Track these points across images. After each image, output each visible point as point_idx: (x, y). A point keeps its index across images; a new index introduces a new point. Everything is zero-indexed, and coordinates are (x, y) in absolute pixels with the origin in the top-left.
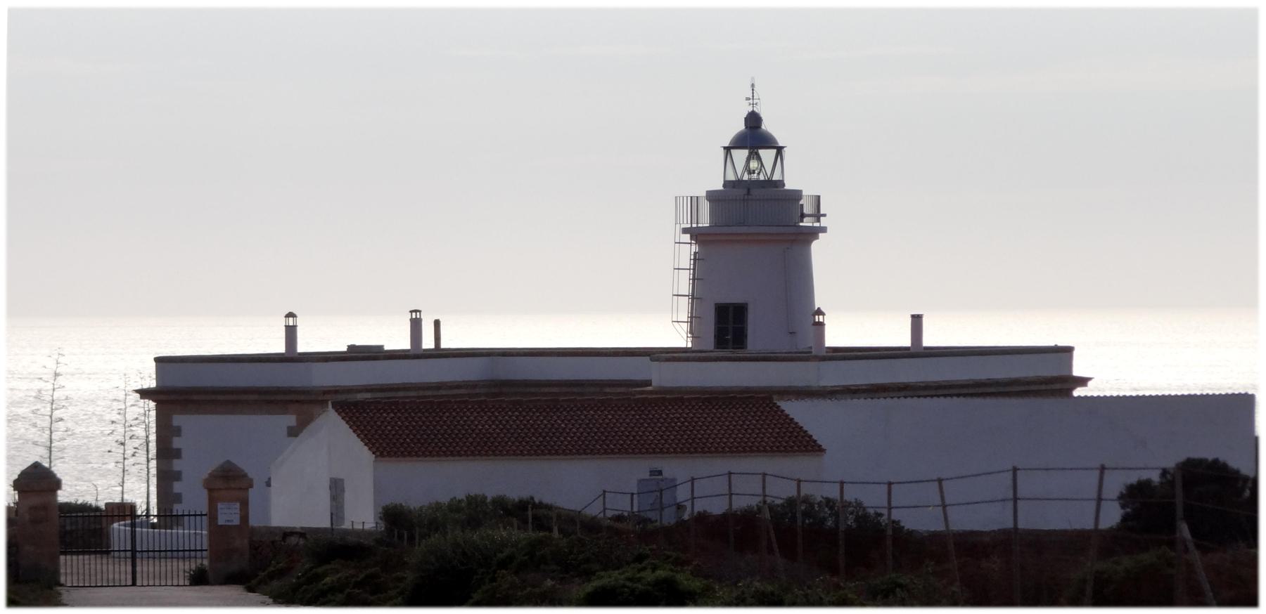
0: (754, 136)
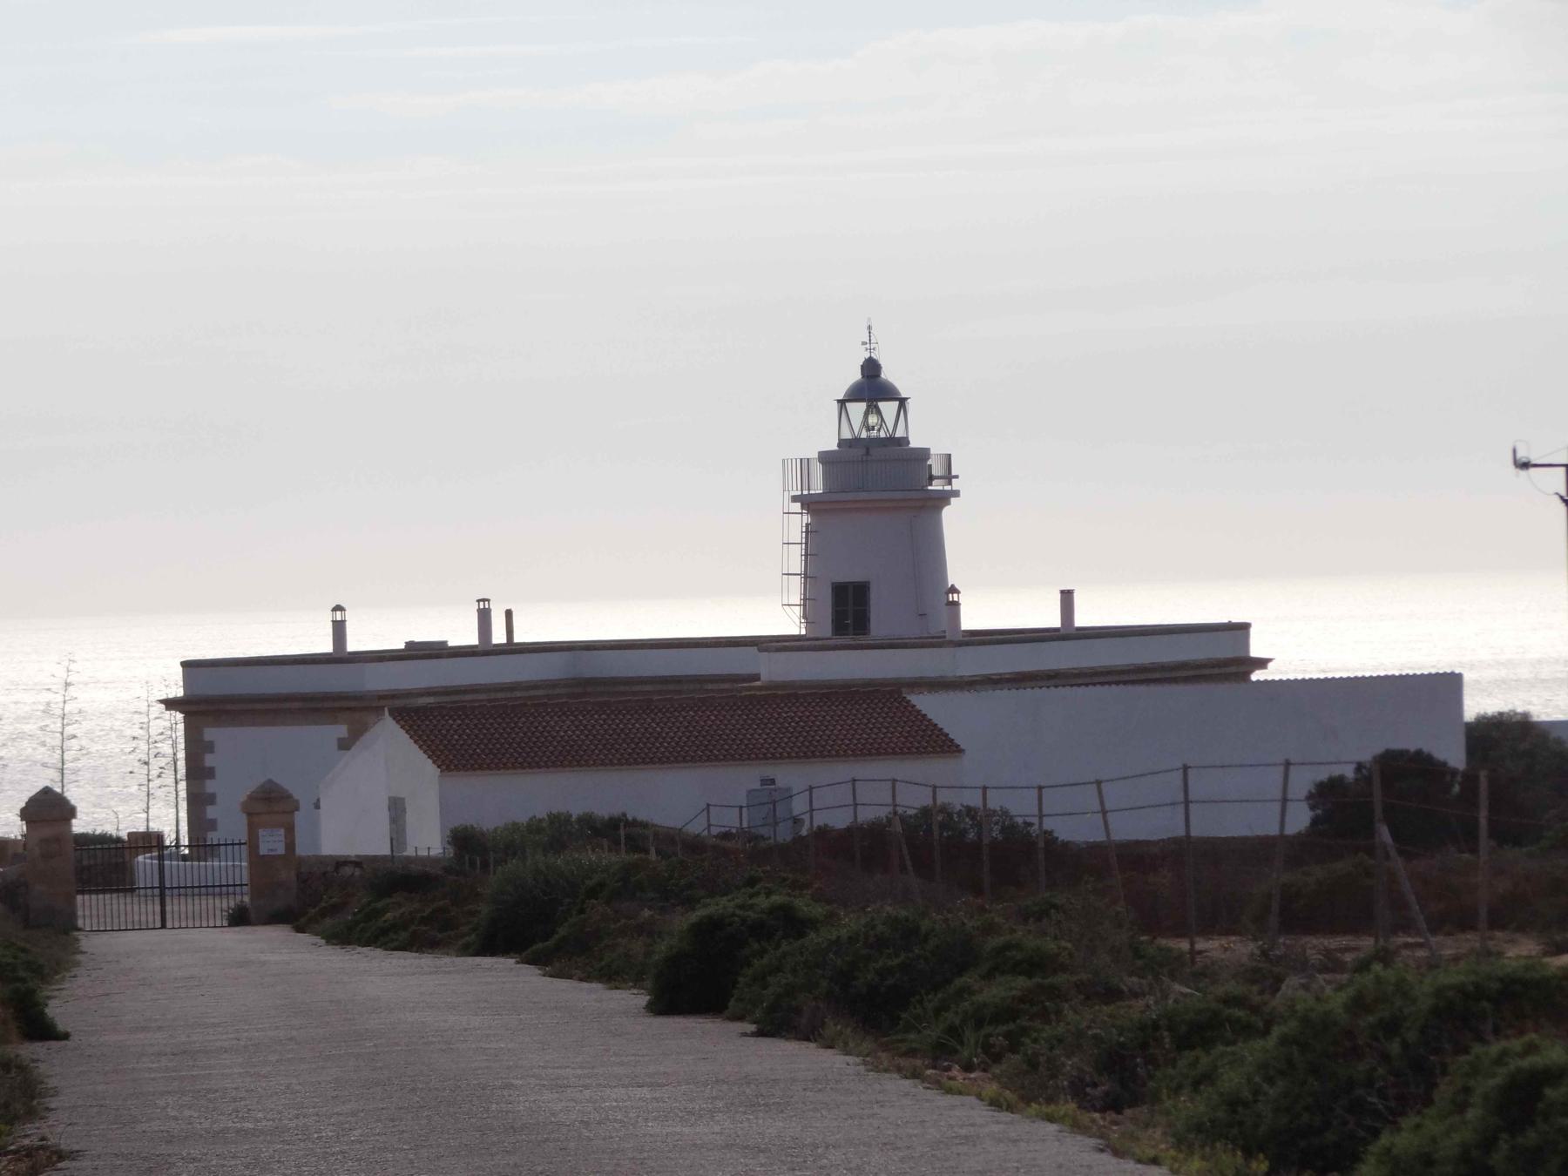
0: (872, 387)
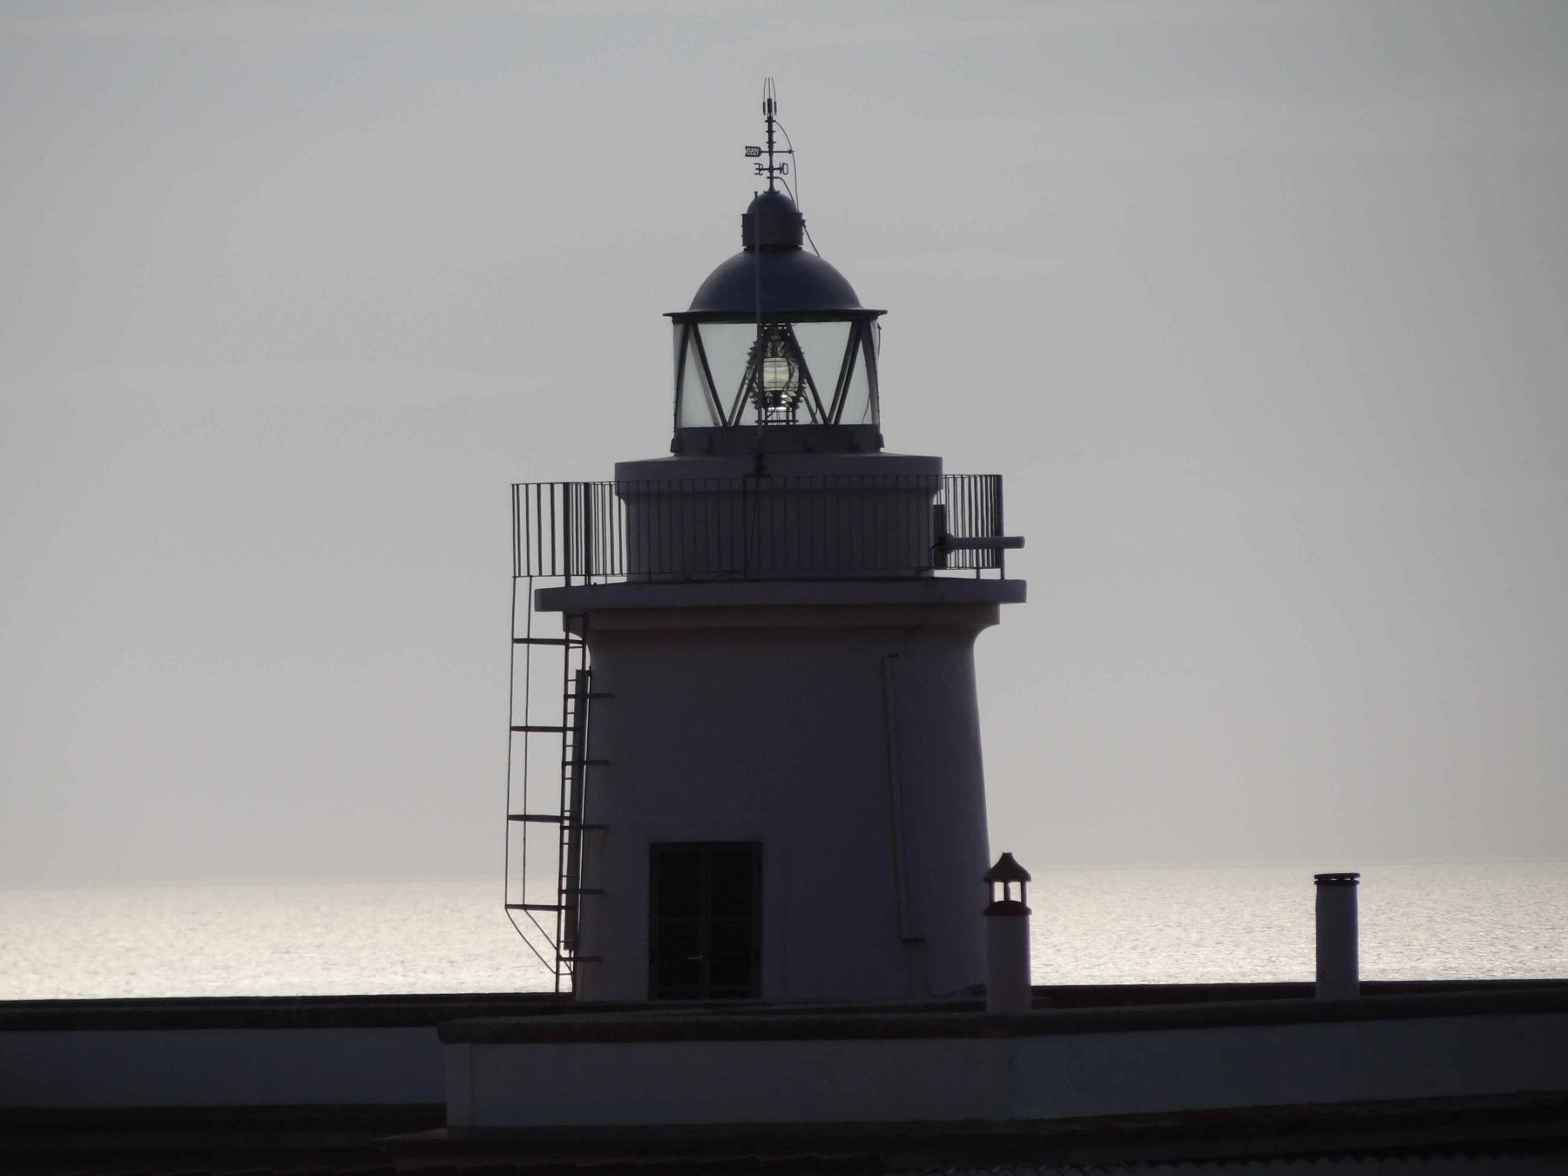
0: (774, 277)
